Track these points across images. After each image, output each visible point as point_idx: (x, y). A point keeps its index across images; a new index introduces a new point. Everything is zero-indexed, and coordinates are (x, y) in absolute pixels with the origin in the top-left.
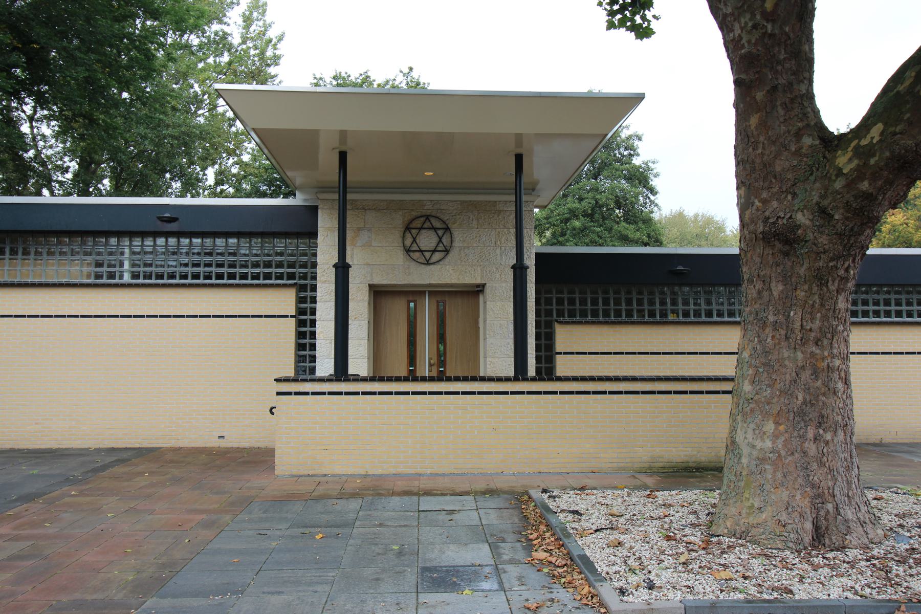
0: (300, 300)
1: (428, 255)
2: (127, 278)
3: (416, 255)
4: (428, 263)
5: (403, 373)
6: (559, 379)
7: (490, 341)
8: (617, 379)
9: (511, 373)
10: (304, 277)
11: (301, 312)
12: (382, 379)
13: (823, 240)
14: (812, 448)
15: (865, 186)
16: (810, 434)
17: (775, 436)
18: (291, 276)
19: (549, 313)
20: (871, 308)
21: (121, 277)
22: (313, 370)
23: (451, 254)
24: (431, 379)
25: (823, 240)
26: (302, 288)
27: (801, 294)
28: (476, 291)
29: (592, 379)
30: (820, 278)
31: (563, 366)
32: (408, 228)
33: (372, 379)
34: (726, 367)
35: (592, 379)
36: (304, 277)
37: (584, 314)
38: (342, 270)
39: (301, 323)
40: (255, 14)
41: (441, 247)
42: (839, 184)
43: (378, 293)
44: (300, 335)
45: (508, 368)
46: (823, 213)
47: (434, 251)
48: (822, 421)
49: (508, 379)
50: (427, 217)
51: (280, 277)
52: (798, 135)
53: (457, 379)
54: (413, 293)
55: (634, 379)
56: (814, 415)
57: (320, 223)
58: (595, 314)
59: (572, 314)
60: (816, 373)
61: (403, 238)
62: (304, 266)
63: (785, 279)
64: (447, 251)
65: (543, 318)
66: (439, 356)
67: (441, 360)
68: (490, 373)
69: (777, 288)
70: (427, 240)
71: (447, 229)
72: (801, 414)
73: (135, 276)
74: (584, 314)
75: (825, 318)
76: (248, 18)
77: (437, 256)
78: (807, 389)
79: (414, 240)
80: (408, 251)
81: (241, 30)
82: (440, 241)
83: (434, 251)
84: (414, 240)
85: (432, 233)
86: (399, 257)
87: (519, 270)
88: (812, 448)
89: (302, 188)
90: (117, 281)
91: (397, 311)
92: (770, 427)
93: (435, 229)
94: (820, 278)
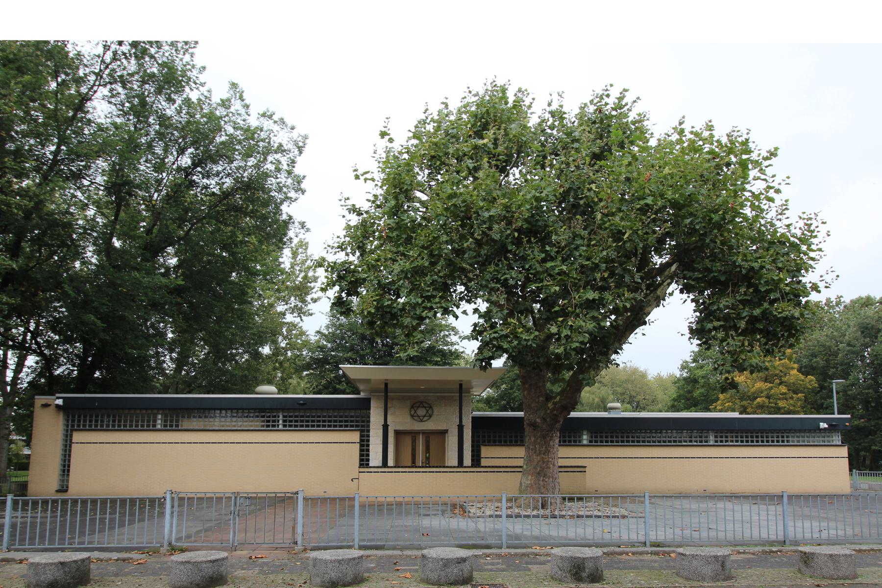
0: (361, 436)
1: (421, 418)
2: (281, 427)
3: (416, 418)
4: (422, 421)
5: (410, 465)
6: (483, 467)
7: (450, 453)
8: (500, 467)
9: (456, 465)
10: (363, 426)
11: (362, 441)
12: (399, 467)
13: (544, 426)
14: (541, 483)
15: (555, 412)
16: (541, 479)
17: (531, 480)
18: (357, 426)
19: (478, 441)
20: (631, 439)
21: (278, 426)
22: (368, 464)
23: (432, 418)
24: (423, 467)
25: (544, 426)
26: (362, 431)
27: (539, 441)
28: (444, 433)
29: (489, 467)
30: (544, 437)
31: (484, 462)
32: (412, 407)
33: (395, 467)
34: (520, 462)
35: (489, 467)
36: (363, 426)
37: (511, 441)
38: (385, 427)
39: (361, 446)
40: (300, 250)
41: (428, 415)
42: (549, 411)
43: (398, 433)
44: (361, 450)
45: (456, 463)
46: (544, 419)
47: (424, 416)
48: (545, 476)
49: (454, 467)
50: (421, 403)
51: (352, 426)
52: (538, 397)
53: (433, 467)
54: (414, 434)
55: (507, 467)
56: (543, 474)
57: (372, 405)
58: (516, 441)
59: (495, 441)
60: (544, 462)
61: (410, 411)
62: (363, 421)
63: (535, 436)
64: (430, 416)
65: (475, 443)
66: (426, 458)
67: (428, 459)
68: (449, 465)
69: (533, 439)
70: (421, 412)
71: (431, 407)
72: (539, 473)
73: (285, 426)
74: (505, 441)
75: (546, 447)
76: (295, 252)
77: (426, 418)
78: (541, 467)
79: (415, 412)
80: (412, 416)
81: (290, 260)
82: (427, 412)
83: (424, 416)
84: (415, 412)
85: (424, 409)
86: (408, 419)
87: (461, 428)
88: (541, 483)
89: (363, 391)
90: (276, 428)
91: (407, 442)
92: (530, 477)
93: (425, 407)
94: (544, 437)
